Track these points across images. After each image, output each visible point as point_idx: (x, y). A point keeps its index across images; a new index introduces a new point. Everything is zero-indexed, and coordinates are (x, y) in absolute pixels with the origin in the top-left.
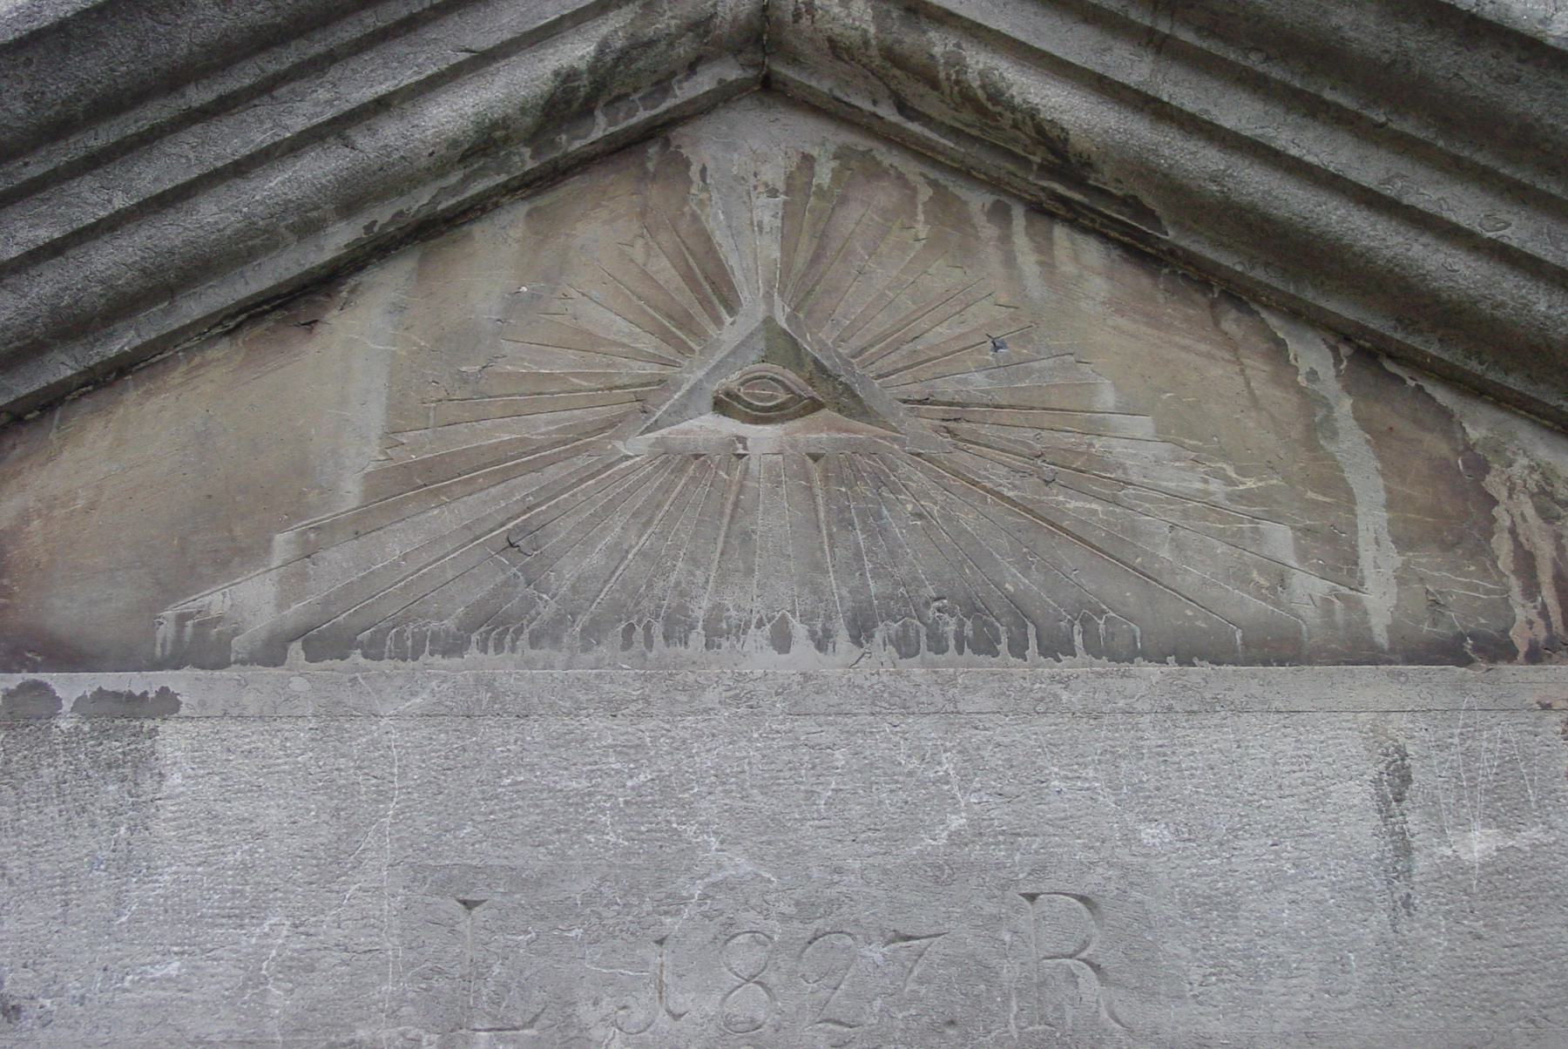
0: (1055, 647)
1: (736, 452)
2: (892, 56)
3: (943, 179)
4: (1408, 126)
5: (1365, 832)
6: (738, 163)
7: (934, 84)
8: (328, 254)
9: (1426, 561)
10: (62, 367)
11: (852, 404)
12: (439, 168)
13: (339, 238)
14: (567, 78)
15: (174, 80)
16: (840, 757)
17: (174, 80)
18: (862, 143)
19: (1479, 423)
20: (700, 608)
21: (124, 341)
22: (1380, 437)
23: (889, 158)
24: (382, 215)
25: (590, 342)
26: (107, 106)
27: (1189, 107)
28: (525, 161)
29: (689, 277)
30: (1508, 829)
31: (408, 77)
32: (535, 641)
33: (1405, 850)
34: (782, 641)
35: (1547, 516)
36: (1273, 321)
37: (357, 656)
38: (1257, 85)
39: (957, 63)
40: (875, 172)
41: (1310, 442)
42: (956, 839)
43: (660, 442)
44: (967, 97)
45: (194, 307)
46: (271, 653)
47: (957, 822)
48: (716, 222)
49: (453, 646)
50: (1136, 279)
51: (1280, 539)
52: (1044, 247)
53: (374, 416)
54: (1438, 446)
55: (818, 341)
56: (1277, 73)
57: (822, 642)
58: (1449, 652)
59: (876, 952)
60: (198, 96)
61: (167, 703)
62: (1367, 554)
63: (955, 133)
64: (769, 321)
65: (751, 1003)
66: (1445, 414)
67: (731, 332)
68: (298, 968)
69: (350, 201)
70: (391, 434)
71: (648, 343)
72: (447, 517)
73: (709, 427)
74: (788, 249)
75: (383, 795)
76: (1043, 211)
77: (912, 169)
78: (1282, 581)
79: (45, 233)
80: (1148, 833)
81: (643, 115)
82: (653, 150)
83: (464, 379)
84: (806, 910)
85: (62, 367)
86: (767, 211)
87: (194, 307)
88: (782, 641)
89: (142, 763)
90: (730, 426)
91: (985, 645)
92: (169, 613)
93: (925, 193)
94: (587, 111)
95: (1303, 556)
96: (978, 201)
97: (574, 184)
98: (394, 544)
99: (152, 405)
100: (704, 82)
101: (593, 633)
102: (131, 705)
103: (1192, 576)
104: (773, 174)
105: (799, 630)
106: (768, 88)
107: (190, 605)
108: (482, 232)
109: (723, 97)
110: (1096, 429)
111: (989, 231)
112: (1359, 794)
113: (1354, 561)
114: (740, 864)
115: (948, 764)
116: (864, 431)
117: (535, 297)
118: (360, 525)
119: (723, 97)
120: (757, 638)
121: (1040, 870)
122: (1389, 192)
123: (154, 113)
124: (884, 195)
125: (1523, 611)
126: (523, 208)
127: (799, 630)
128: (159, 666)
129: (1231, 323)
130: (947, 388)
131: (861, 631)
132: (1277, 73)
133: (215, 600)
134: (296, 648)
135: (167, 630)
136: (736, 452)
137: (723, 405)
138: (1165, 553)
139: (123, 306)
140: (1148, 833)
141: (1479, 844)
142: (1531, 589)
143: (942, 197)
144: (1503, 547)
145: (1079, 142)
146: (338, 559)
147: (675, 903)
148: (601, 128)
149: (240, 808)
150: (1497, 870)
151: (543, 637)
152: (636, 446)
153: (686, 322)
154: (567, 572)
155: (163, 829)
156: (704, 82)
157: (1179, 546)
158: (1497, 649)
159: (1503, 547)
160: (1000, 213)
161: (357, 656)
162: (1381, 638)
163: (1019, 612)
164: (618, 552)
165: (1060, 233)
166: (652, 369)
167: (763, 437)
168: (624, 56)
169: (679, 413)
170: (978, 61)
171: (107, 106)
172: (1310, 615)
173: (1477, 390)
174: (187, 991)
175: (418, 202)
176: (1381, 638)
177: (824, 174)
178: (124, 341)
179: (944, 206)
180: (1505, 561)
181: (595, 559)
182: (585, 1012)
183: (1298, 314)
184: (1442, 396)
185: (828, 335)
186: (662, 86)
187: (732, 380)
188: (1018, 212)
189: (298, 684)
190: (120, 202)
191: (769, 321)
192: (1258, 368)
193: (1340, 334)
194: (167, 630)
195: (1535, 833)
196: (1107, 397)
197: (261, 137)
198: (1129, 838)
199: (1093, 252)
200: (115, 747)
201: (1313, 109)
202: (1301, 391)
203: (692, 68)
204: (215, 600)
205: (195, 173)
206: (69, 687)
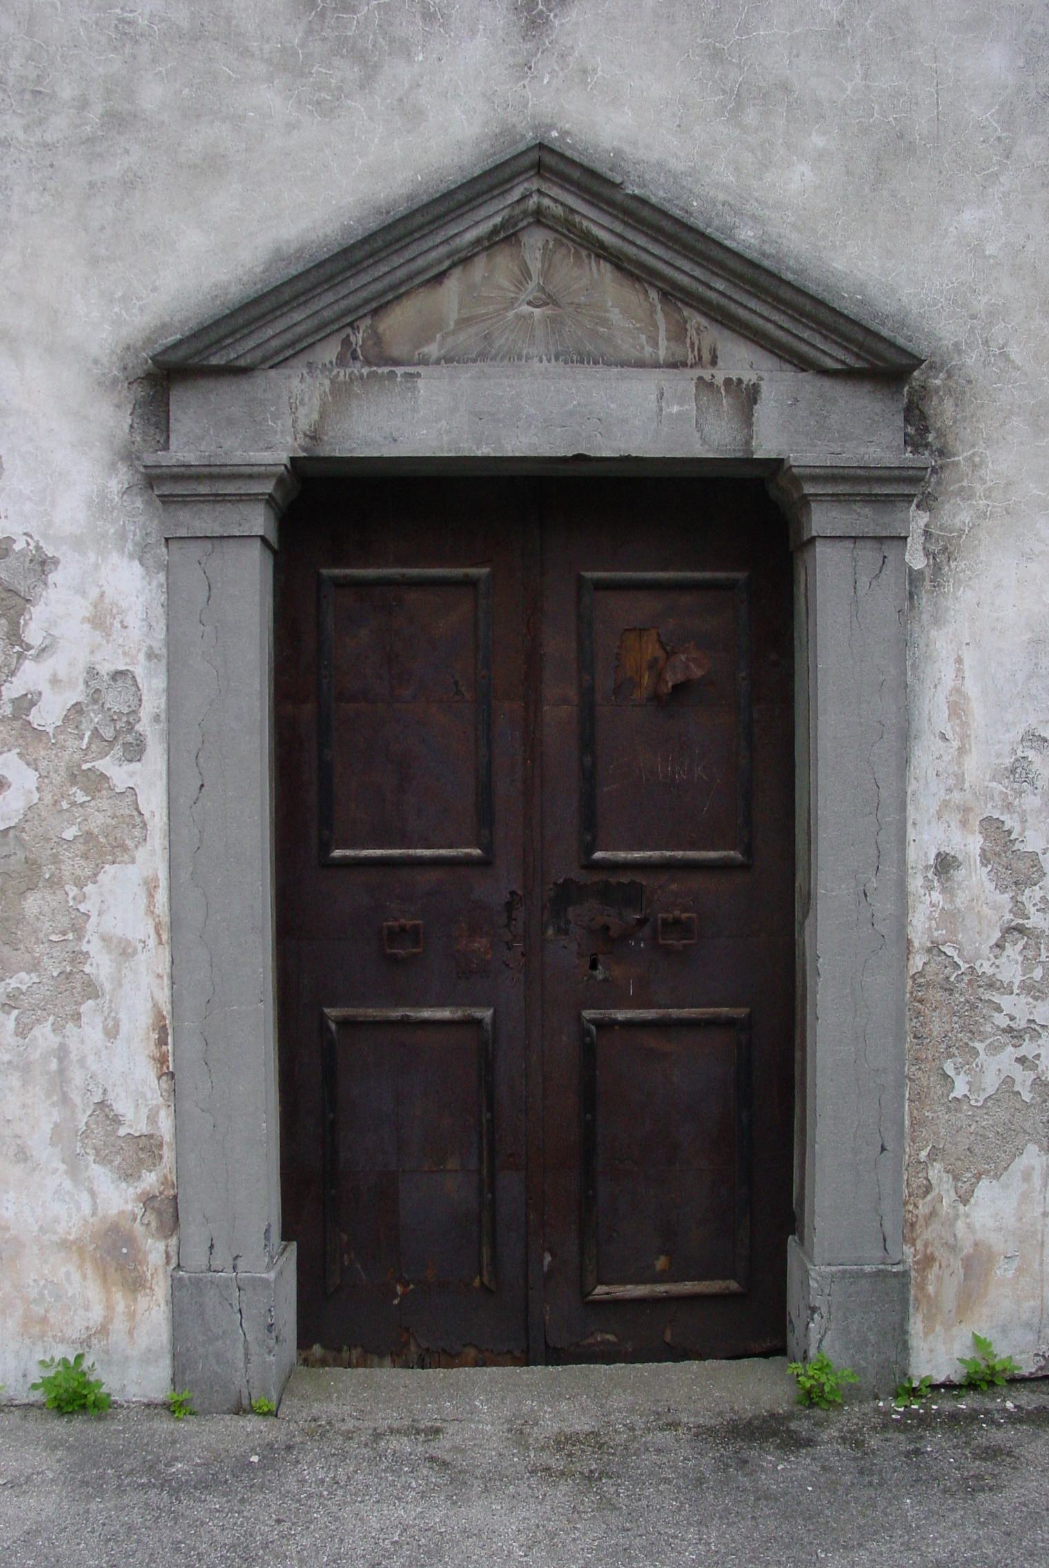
0: (596, 363)
1: (531, 315)
2: (566, 220)
3: (577, 247)
4: (676, 247)
5: (653, 406)
6: (532, 241)
7: (575, 226)
8: (444, 268)
9: (673, 344)
10: (390, 296)
11: (556, 304)
12: (468, 247)
13: (447, 264)
14: (495, 226)
15: (411, 233)
16: (552, 388)
17: (411, 233)
18: (559, 237)
19: (687, 312)
20: (524, 353)
21: (402, 290)
22: (666, 315)
23: (565, 241)
24: (456, 258)
25: (501, 288)
26: (398, 240)
27: (631, 239)
28: (486, 244)
29: (521, 271)
30: (682, 406)
31: (461, 229)
32: (491, 359)
33: (661, 410)
34: (541, 361)
35: (698, 334)
36: (646, 285)
37: (455, 363)
38: (646, 235)
39: (581, 223)
40: (562, 244)
41: (651, 315)
42: (575, 406)
43: (516, 313)
44: (582, 231)
45: (417, 281)
46: (438, 362)
47: (575, 403)
48: (527, 257)
49: (474, 361)
50: (618, 274)
51: (643, 337)
52: (598, 264)
53: (455, 306)
54: (677, 316)
55: (550, 288)
56: (649, 232)
57: (549, 361)
58: (674, 366)
59: (559, 430)
60: (417, 235)
61: (418, 375)
62: (660, 342)
63: (579, 237)
64: (539, 283)
65: (535, 440)
66: (679, 309)
67: (531, 285)
68: (448, 432)
69: (449, 256)
70: (459, 312)
71: (513, 288)
72: (472, 330)
73: (526, 309)
74: (543, 266)
75: (463, 396)
76: (598, 256)
77: (570, 244)
78: (643, 348)
79: (387, 269)
80: (612, 406)
81: (511, 231)
82: (513, 238)
83: (474, 297)
84: (545, 421)
85: (390, 296)
86: (538, 255)
87: (417, 281)
88: (541, 361)
89: (414, 389)
90: (530, 309)
91: (582, 362)
92: (417, 353)
93: (573, 250)
94: (499, 232)
95: (647, 342)
96: (584, 253)
97: (496, 247)
98: (461, 337)
99: (409, 303)
100: (525, 223)
101: (502, 359)
102: (411, 375)
103: (625, 347)
104: (540, 245)
105: (544, 357)
106: (539, 223)
107: (420, 351)
108: (476, 259)
109: (529, 225)
110: (607, 311)
111: (586, 261)
112: (653, 397)
113: (657, 343)
114: (533, 411)
115: (574, 390)
116: (558, 311)
117: (488, 276)
118: (454, 333)
119: (529, 225)
120: (536, 360)
121: (590, 413)
122: (671, 261)
123: (408, 240)
124: (563, 251)
125: (690, 356)
126: (485, 253)
127: (544, 357)
128: (415, 365)
129: (637, 286)
130: (576, 300)
131: (557, 359)
132: (649, 232)
133: (426, 350)
134: (443, 362)
135: (417, 356)
136: (531, 315)
137: (529, 303)
138: (619, 342)
139: (402, 283)
140: (612, 406)
141: (675, 409)
142: (693, 351)
143: (577, 253)
144: (688, 341)
145: (606, 243)
146: (450, 342)
147: (520, 419)
148: (502, 235)
149: (434, 398)
150: (679, 414)
151: (492, 359)
152: (511, 314)
153: (521, 283)
154: (497, 345)
155: (420, 402)
156: (525, 223)
157: (622, 340)
158: (684, 365)
159: (688, 341)
160: (589, 256)
161: (455, 363)
162: (662, 362)
163: (589, 354)
164: (507, 339)
165: (602, 261)
166: (513, 295)
167: (537, 311)
168: (508, 221)
169: (520, 305)
170: (585, 223)
171: (398, 240)
172: (648, 355)
173: (687, 304)
174: (990, 1044)
175: (462, 255)
176: (662, 362)
177: (551, 246)
178: (402, 290)
179: (577, 255)
180: (688, 345)
181: (502, 341)
182: (503, 441)
183: (652, 284)
184: (680, 305)
185: (551, 287)
186: (516, 224)
187: (531, 298)
188: (593, 256)
189: (444, 371)
190: (402, 261)
191: (539, 283)
192: (642, 297)
193: (660, 290)
194: (417, 356)
195: (687, 407)
196: (610, 304)
197: (431, 244)
198: (608, 407)
199: (608, 265)
200: (409, 385)
201: (656, 240)
202: (650, 303)
203: (522, 220)
204: (426, 350)
205: (417, 253)
206: (399, 370)
